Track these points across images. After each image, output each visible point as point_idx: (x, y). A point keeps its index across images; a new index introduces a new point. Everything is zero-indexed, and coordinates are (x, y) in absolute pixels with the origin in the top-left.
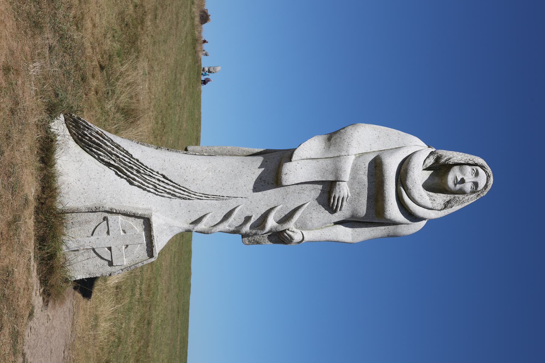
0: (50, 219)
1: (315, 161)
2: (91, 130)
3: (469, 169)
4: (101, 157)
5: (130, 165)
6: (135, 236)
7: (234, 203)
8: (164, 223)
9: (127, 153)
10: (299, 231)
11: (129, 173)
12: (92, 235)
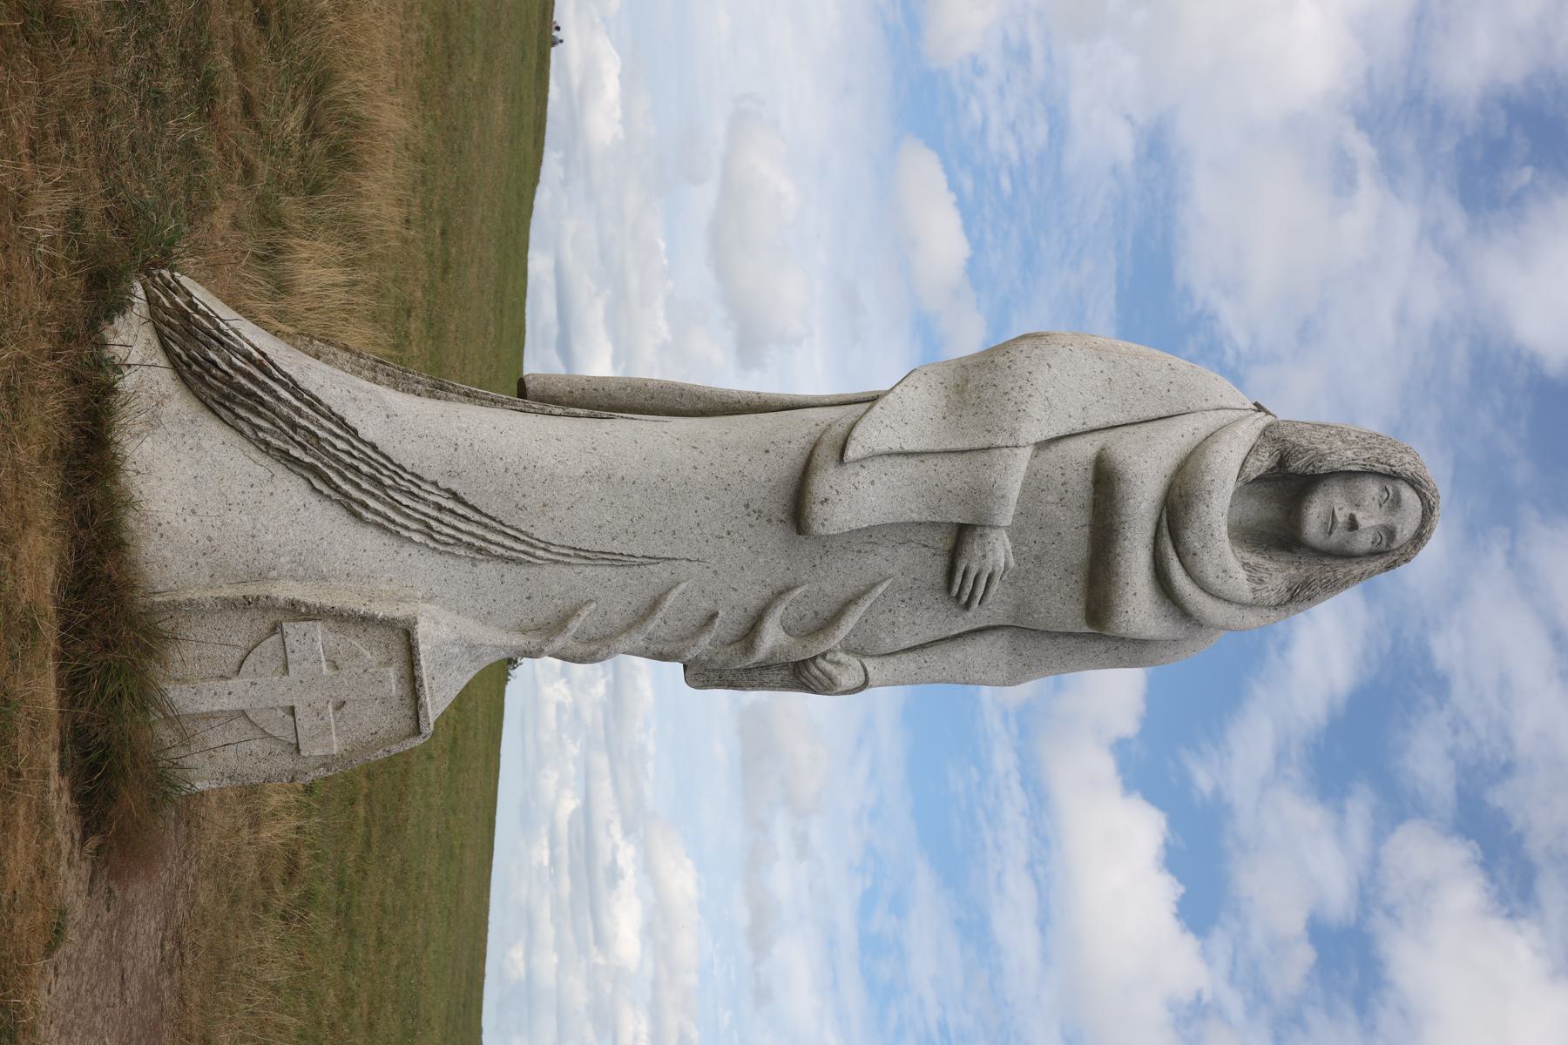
0: (107, 618)
1: (913, 461)
2: (229, 347)
3: (1372, 489)
4: (261, 434)
5: (349, 460)
6: (366, 677)
7: (665, 575)
8: (453, 637)
9: (341, 422)
10: (854, 662)
11: (346, 487)
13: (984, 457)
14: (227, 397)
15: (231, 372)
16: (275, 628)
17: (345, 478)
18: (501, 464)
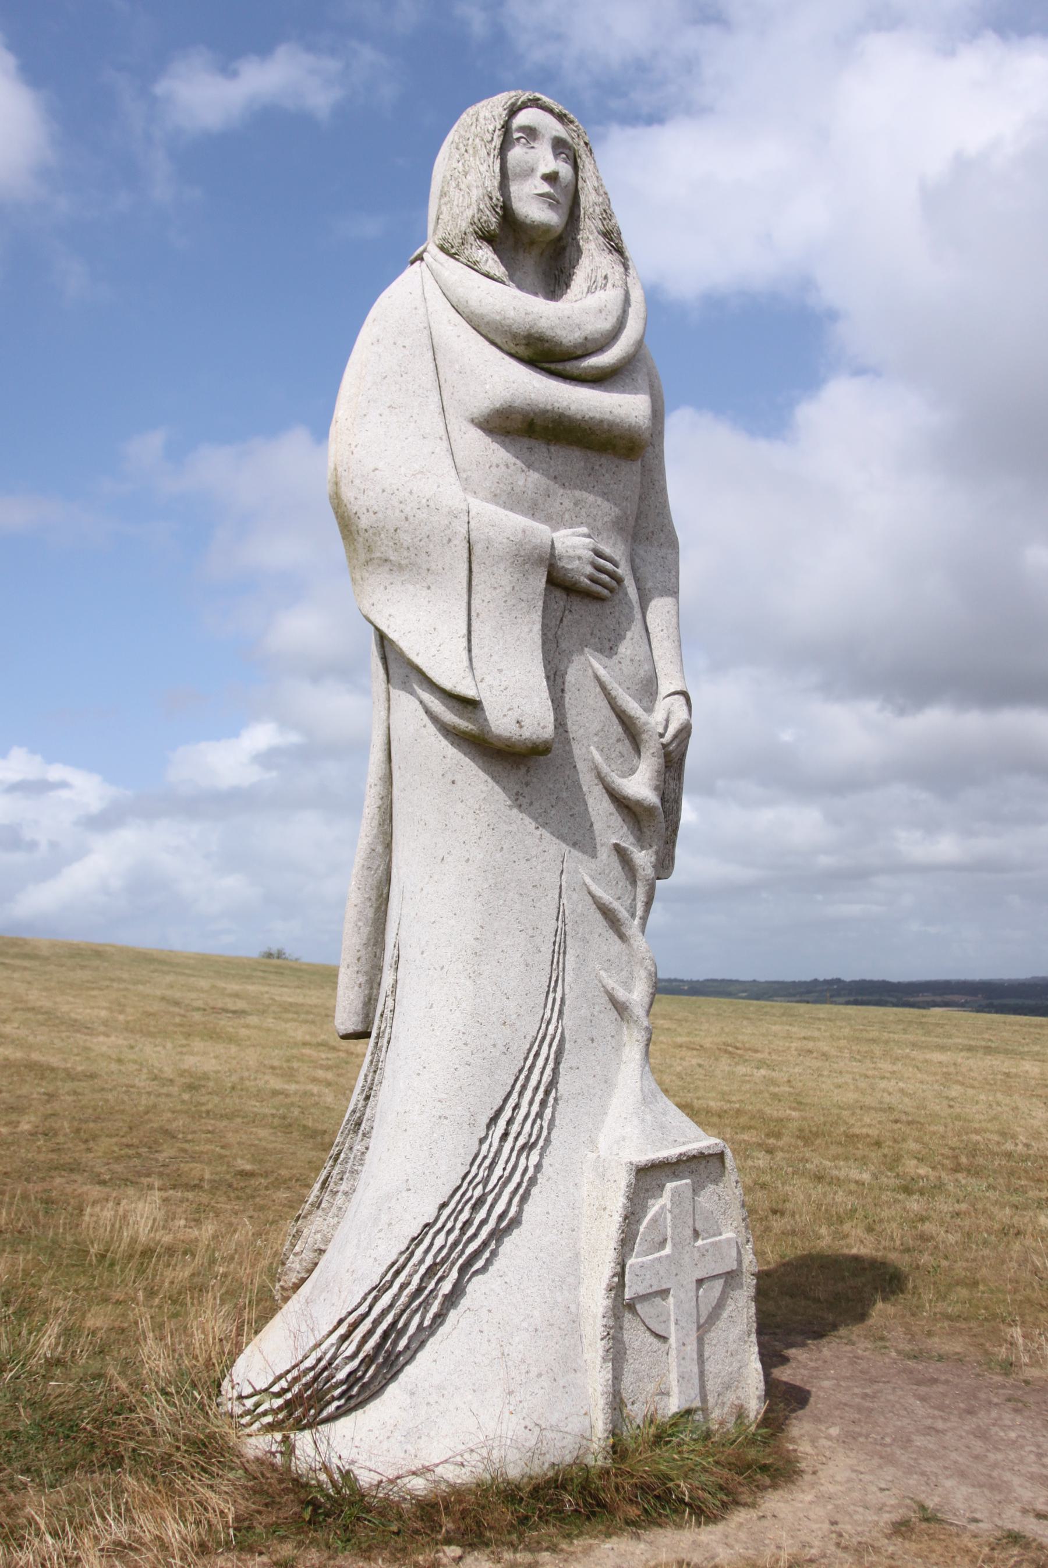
2: (334, 1357)
4: (426, 1323)
5: (457, 1232)
9: (416, 1240)
12: (664, 1339)
13: (477, 550)
14: (386, 1359)
15: (361, 1356)
16: (631, 1307)
17: (475, 1235)
18: (461, 1070)
